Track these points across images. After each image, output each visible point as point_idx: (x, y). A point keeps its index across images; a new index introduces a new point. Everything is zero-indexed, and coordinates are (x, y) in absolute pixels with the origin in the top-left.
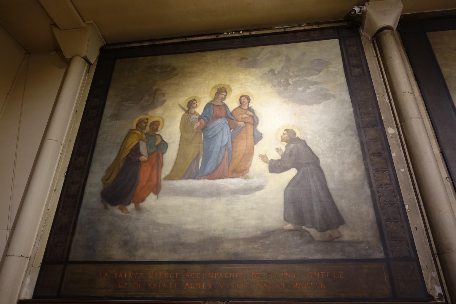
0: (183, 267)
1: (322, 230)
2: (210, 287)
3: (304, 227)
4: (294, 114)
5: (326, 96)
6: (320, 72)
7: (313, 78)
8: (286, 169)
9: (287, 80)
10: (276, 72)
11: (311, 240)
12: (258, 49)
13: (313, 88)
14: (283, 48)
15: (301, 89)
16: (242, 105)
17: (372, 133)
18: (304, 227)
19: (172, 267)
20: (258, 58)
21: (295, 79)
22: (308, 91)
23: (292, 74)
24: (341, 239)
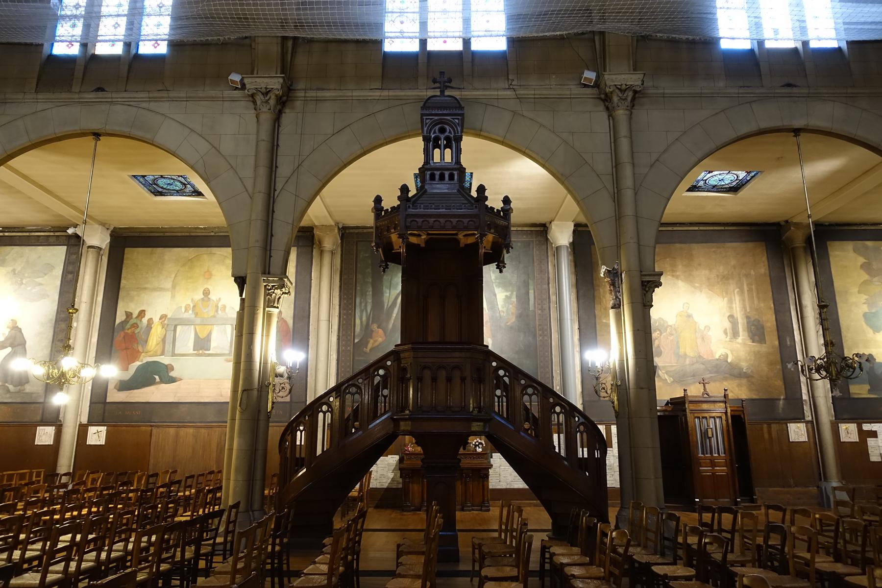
0: (24, 406)
1: (15, 386)
2: (481, 444)
3: (7, 384)
4: (444, 72)
5: (44, 296)
6: (45, 275)
7: (39, 280)
8: (6, 347)
9: (22, 279)
10: (16, 272)
11: (8, 391)
12: (9, 248)
13: (38, 288)
14: (27, 250)
15: (29, 288)
16: (263, 94)
17: (63, 325)
18: (7, 384)
19: (20, 405)
20: (7, 257)
21: (28, 279)
22: (34, 290)
23: (26, 275)
24: (24, 391)
